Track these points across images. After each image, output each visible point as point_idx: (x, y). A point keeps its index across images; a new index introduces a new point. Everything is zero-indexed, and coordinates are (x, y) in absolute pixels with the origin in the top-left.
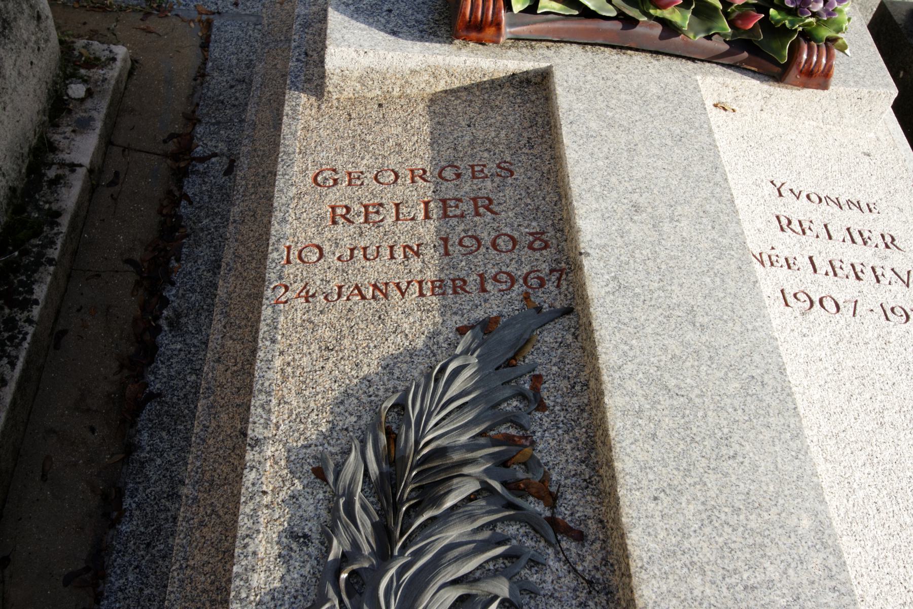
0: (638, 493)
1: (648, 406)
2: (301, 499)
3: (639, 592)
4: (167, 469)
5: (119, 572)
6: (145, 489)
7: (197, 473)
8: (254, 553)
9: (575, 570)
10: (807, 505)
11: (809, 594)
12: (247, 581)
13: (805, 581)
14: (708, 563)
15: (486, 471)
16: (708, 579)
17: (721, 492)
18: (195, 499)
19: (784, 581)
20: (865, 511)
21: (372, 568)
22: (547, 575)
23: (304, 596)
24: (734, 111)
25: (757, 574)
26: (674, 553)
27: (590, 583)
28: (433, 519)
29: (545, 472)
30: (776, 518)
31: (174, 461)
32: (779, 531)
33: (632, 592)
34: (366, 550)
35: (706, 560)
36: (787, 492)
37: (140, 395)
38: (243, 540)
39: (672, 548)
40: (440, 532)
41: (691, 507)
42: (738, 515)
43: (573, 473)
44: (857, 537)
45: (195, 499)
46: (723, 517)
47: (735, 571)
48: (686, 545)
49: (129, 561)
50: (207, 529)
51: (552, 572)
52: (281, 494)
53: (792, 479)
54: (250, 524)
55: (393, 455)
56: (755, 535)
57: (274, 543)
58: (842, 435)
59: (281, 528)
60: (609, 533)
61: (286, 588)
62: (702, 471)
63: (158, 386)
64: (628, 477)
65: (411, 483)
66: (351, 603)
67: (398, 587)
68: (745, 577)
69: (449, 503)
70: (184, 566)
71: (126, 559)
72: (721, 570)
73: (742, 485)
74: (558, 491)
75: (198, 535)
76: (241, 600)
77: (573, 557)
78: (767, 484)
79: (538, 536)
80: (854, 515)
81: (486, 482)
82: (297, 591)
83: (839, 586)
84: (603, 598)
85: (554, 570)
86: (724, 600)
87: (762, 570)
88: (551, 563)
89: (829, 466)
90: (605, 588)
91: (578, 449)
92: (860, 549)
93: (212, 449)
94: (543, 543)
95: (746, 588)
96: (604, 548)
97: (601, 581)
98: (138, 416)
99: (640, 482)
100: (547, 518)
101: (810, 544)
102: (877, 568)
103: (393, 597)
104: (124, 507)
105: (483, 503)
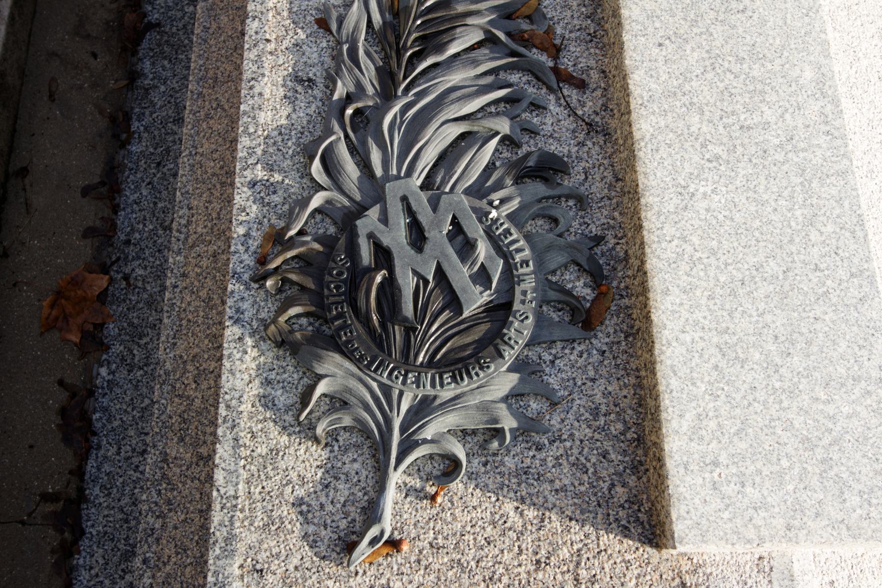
0: (642, 39)
2: (305, 47)
3: (638, 126)
4: (171, 96)
5: (132, 187)
6: (151, 114)
7: (200, 70)
8: (260, 94)
9: (576, 114)
10: (812, 58)
11: (803, 136)
12: (254, 118)
13: (800, 125)
14: (707, 105)
15: (490, 22)
16: (706, 118)
17: (727, 42)
18: (200, 94)
19: (780, 124)
20: (867, 78)
21: (376, 107)
22: (548, 118)
23: (310, 132)
25: (754, 116)
26: (675, 94)
27: (589, 124)
28: (436, 65)
29: (549, 26)
30: (779, 68)
31: (178, 88)
32: (781, 80)
33: (630, 126)
34: (370, 90)
35: (705, 101)
36: (793, 46)
37: (138, 25)
38: (249, 82)
39: (673, 90)
40: (443, 76)
41: (695, 54)
42: (741, 64)
43: (578, 27)
44: (856, 100)
45: (200, 94)
46: (726, 65)
47: (733, 113)
48: (687, 87)
49: (142, 178)
50: (213, 121)
51: (553, 116)
52: (284, 42)
53: (799, 35)
54: (254, 68)
55: (396, 7)
56: (756, 82)
57: (280, 86)
58: (855, 8)
59: (286, 73)
60: (610, 82)
61: (293, 125)
62: (709, 22)
63: (156, 16)
64: (634, 24)
65: (414, 32)
66: (356, 137)
67: (402, 123)
68: (742, 118)
69: (453, 50)
70: (194, 153)
71: (139, 176)
72: (719, 111)
73: (748, 38)
74: (562, 44)
75: (205, 127)
76: (250, 135)
77: (574, 103)
78: (774, 38)
79: (540, 83)
80: (855, 81)
81: (490, 32)
82: (303, 128)
83: (832, 130)
84: (601, 139)
85: (554, 113)
86: (719, 137)
87: (759, 113)
88: (552, 108)
89: (837, 35)
90: (603, 130)
91: (584, 5)
92: (857, 111)
93: (213, 49)
94: (544, 90)
95: (742, 127)
96: (605, 96)
97: (600, 124)
98: (139, 45)
99: (645, 29)
100: (551, 68)
101: (809, 93)
102: (870, 128)
103: (397, 132)
104: (132, 130)
105: (487, 51)
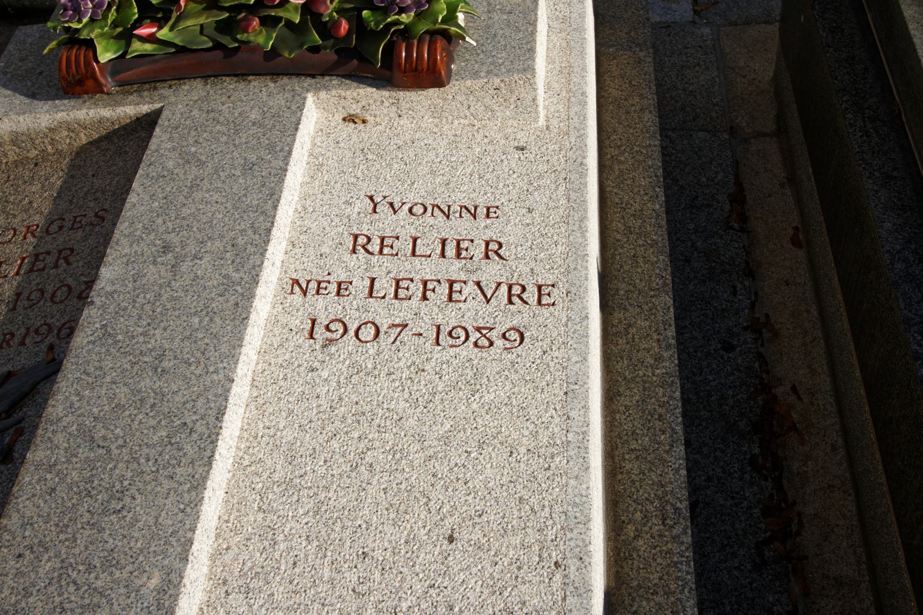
1: (64, 460)
24: (364, 122)
